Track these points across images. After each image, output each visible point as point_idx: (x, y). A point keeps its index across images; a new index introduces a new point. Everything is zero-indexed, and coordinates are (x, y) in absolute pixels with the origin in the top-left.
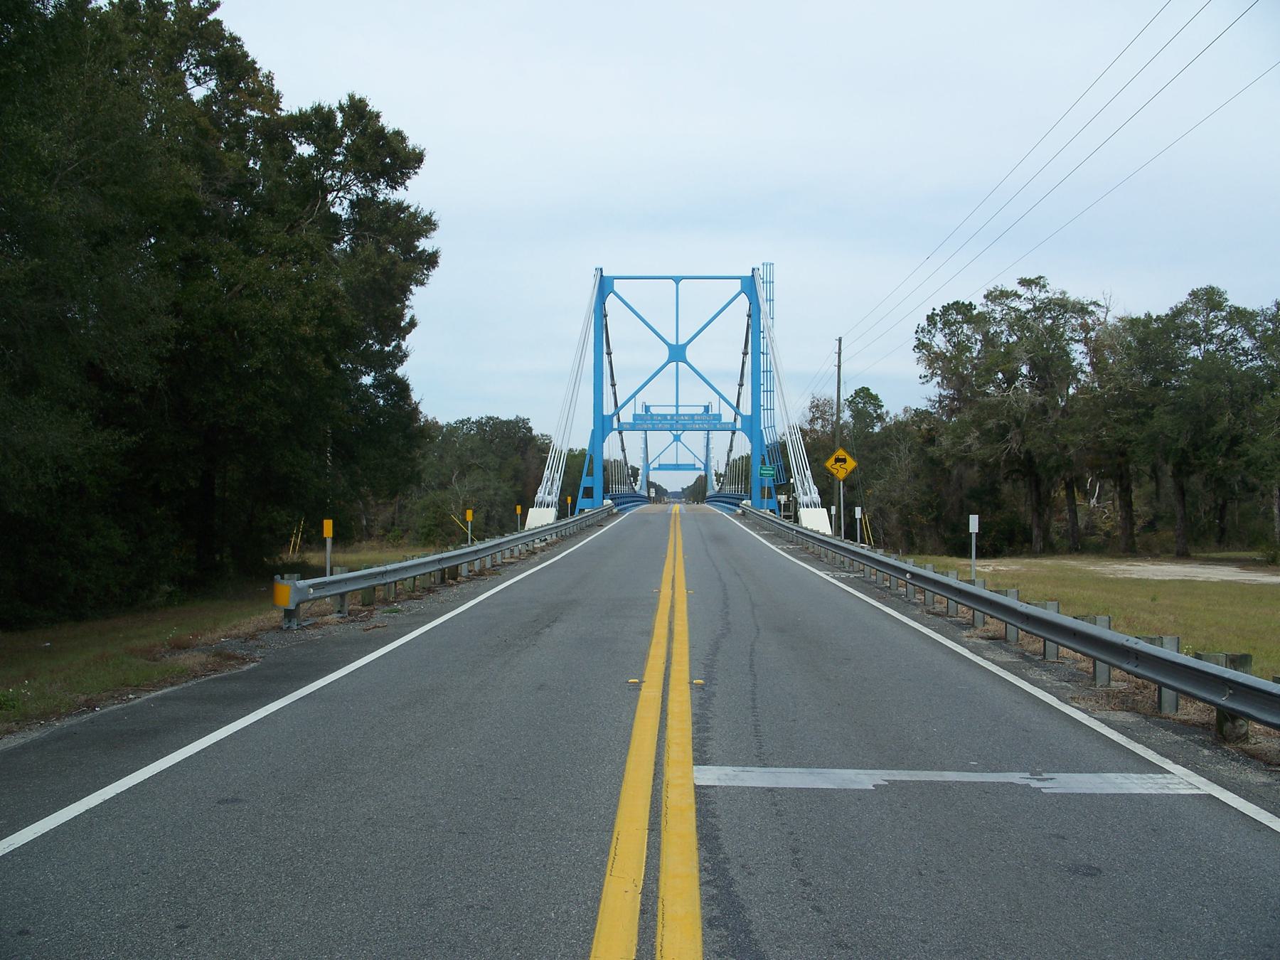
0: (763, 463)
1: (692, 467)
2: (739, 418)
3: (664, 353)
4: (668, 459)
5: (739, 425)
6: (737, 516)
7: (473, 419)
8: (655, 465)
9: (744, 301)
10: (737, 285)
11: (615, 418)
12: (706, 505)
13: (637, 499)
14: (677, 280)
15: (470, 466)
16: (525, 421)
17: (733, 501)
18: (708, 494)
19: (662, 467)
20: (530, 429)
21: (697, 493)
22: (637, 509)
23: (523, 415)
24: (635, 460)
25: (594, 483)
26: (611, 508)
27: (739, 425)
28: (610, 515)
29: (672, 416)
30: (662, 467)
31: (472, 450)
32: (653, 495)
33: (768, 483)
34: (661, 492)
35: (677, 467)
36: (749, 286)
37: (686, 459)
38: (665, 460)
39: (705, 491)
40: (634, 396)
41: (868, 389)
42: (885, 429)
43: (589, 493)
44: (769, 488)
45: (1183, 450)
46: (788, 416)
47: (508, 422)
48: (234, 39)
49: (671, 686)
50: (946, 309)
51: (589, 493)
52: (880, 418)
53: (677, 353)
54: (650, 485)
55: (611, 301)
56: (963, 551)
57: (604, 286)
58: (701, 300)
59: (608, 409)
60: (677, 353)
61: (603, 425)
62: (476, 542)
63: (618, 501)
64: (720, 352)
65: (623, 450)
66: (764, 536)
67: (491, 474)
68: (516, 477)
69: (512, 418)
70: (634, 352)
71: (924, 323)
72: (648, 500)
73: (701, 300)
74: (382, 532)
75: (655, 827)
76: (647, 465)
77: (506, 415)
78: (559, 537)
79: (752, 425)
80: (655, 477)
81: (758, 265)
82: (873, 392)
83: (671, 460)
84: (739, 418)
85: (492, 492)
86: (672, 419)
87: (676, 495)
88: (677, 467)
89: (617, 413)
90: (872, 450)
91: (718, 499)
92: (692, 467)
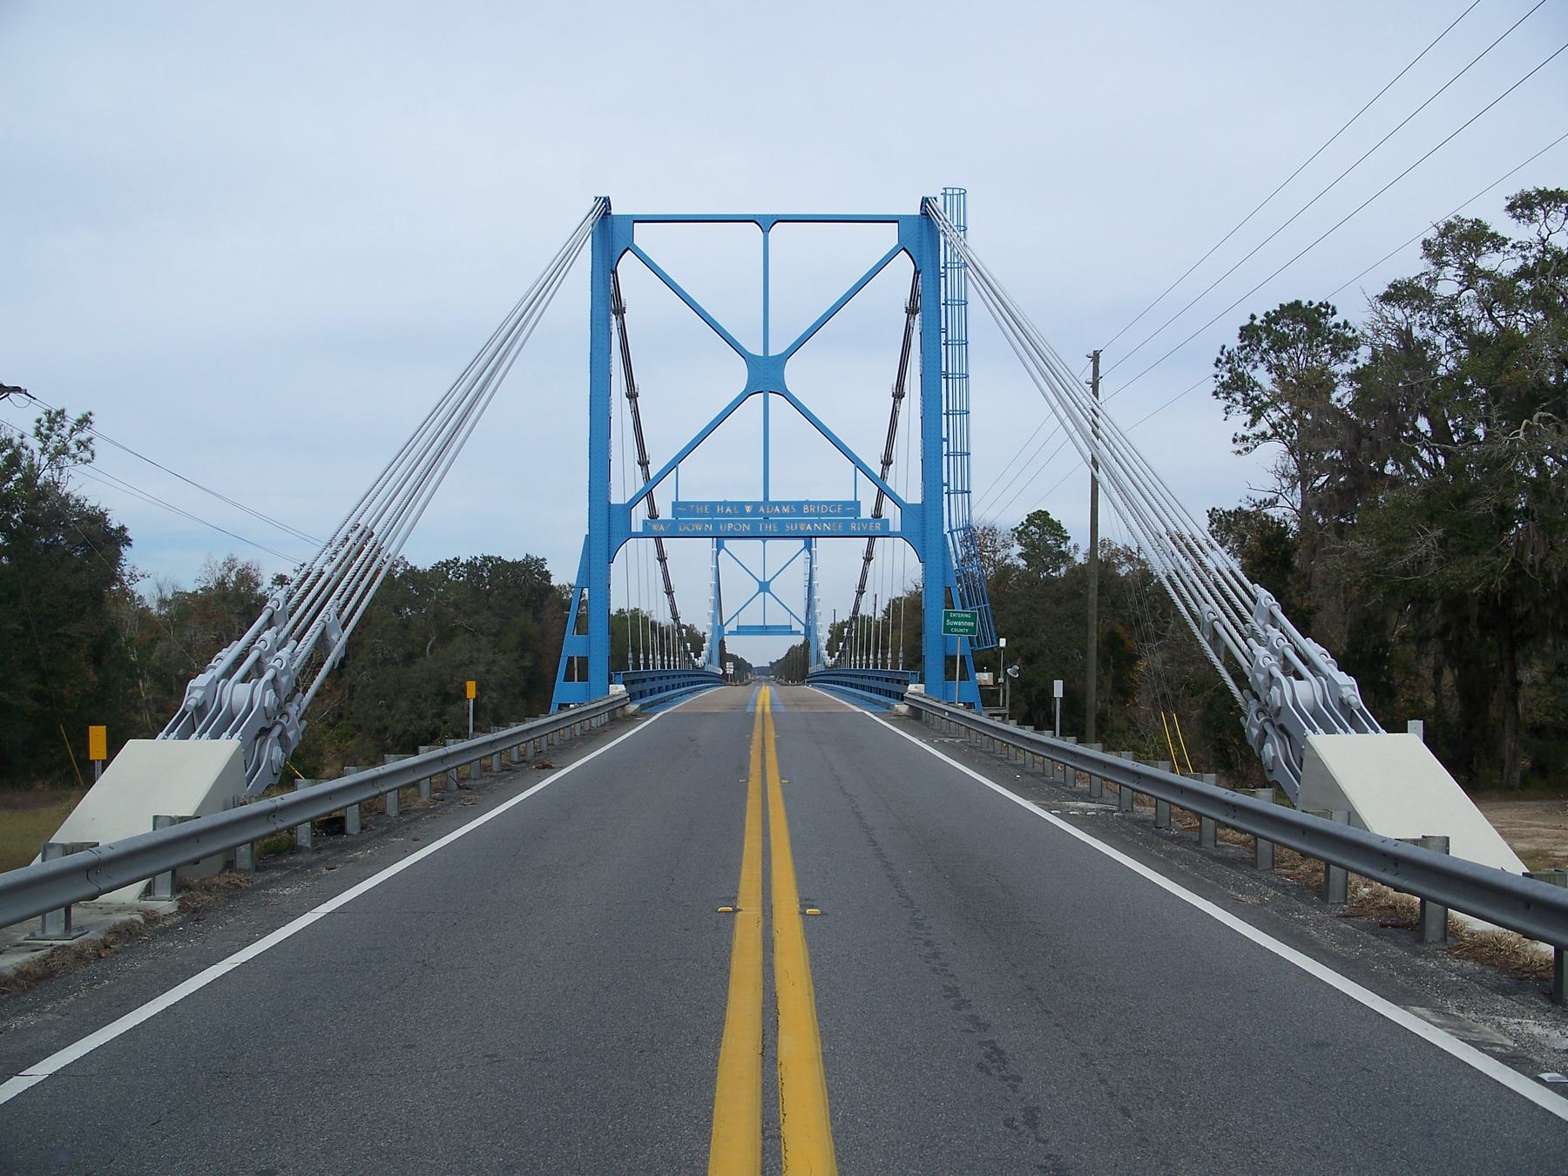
0: (949, 603)
4: (752, 617)
6: (898, 719)
7: (463, 561)
8: (732, 627)
9: (903, 266)
10: (889, 235)
12: (809, 687)
13: (701, 678)
14: (766, 223)
15: (452, 630)
16: (540, 563)
17: (886, 688)
18: (812, 669)
19: (741, 630)
20: (547, 576)
21: (794, 668)
22: (690, 699)
24: (696, 616)
25: (655, 659)
26: (620, 704)
28: (617, 718)
29: (755, 505)
30: (741, 630)
31: (456, 605)
32: (730, 671)
33: (960, 648)
34: (741, 665)
35: (765, 630)
36: (923, 233)
37: (777, 617)
38: (747, 619)
39: (806, 664)
40: (673, 465)
42: (1072, 571)
43: (580, 670)
44: (962, 658)
47: (515, 564)
50: (1271, 319)
51: (580, 670)
52: (1064, 557)
53: (764, 587)
54: (724, 657)
55: (628, 266)
56: (1044, 724)
57: (610, 234)
59: (624, 484)
60: (764, 587)
61: (608, 528)
62: (302, 781)
63: (636, 688)
64: (854, 383)
65: (669, 592)
66: (1081, 821)
67: (484, 641)
68: (524, 644)
70: (682, 384)
71: (1234, 343)
72: (724, 679)
75: (768, 946)
76: (719, 628)
77: (512, 554)
78: (215, 871)
80: (734, 646)
81: (933, 191)
82: (1054, 516)
85: (482, 668)
86: (755, 513)
87: (762, 670)
88: (765, 630)
90: (1058, 602)
91: (829, 678)
92: (839, 520)
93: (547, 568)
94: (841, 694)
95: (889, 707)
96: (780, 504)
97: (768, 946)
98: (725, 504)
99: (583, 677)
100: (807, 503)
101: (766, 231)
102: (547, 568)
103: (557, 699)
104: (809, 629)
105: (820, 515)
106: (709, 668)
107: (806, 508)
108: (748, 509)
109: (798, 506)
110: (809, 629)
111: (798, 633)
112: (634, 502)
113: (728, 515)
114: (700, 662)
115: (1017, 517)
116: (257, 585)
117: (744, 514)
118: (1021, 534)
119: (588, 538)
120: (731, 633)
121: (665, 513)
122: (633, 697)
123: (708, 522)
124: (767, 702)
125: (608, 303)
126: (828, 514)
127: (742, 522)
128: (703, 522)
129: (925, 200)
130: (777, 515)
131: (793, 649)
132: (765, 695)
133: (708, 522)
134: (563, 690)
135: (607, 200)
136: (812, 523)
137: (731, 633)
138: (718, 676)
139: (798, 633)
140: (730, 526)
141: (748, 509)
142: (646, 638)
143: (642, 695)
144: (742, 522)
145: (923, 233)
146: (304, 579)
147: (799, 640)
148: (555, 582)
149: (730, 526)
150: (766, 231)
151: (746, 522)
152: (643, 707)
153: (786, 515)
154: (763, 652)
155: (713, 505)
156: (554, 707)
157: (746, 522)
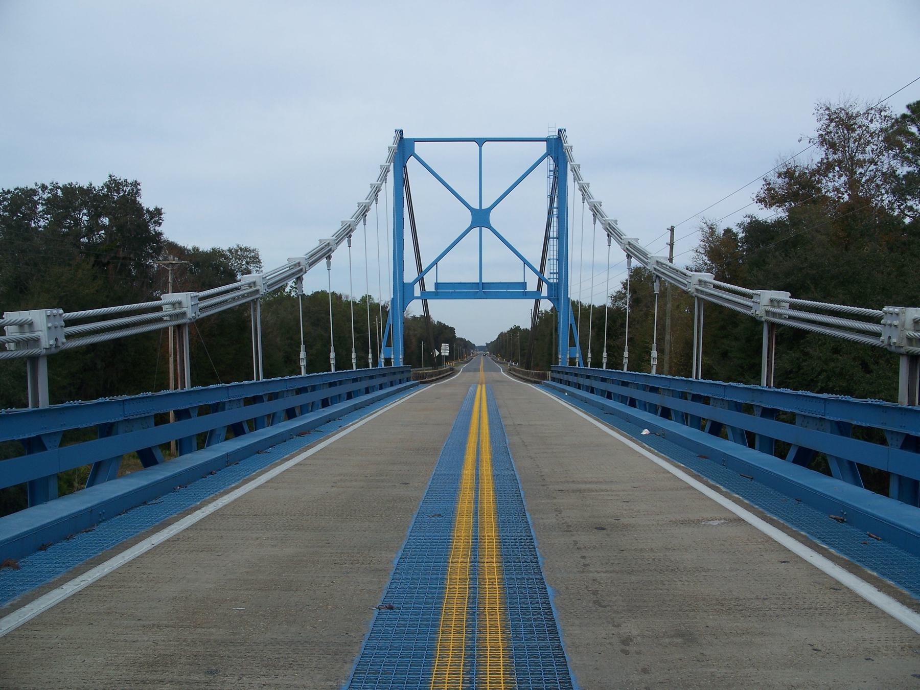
1: (516, 291)
2: (545, 286)
3: (467, 218)
5: (545, 292)
9: (548, 164)
10: (542, 147)
11: (417, 287)
14: (480, 142)
21: (528, 352)
23: (124, 174)
27: (545, 292)
35: (481, 290)
37: (502, 268)
40: (435, 263)
46: (597, 282)
48: (438, 322)
53: (481, 218)
55: (412, 163)
57: (403, 149)
59: (410, 274)
60: (481, 218)
61: (403, 292)
64: (524, 216)
75: (477, 489)
79: (558, 291)
83: (477, 323)
84: (545, 286)
87: (481, 348)
88: (481, 290)
89: (421, 279)
92: (516, 291)
94: (574, 399)
97: (477, 489)
101: (480, 146)
112: (415, 282)
121: (430, 287)
125: (402, 182)
129: (560, 131)
131: (908, 173)
132: (479, 392)
135: (401, 131)
145: (557, 148)
146: (697, 398)
150: (480, 146)
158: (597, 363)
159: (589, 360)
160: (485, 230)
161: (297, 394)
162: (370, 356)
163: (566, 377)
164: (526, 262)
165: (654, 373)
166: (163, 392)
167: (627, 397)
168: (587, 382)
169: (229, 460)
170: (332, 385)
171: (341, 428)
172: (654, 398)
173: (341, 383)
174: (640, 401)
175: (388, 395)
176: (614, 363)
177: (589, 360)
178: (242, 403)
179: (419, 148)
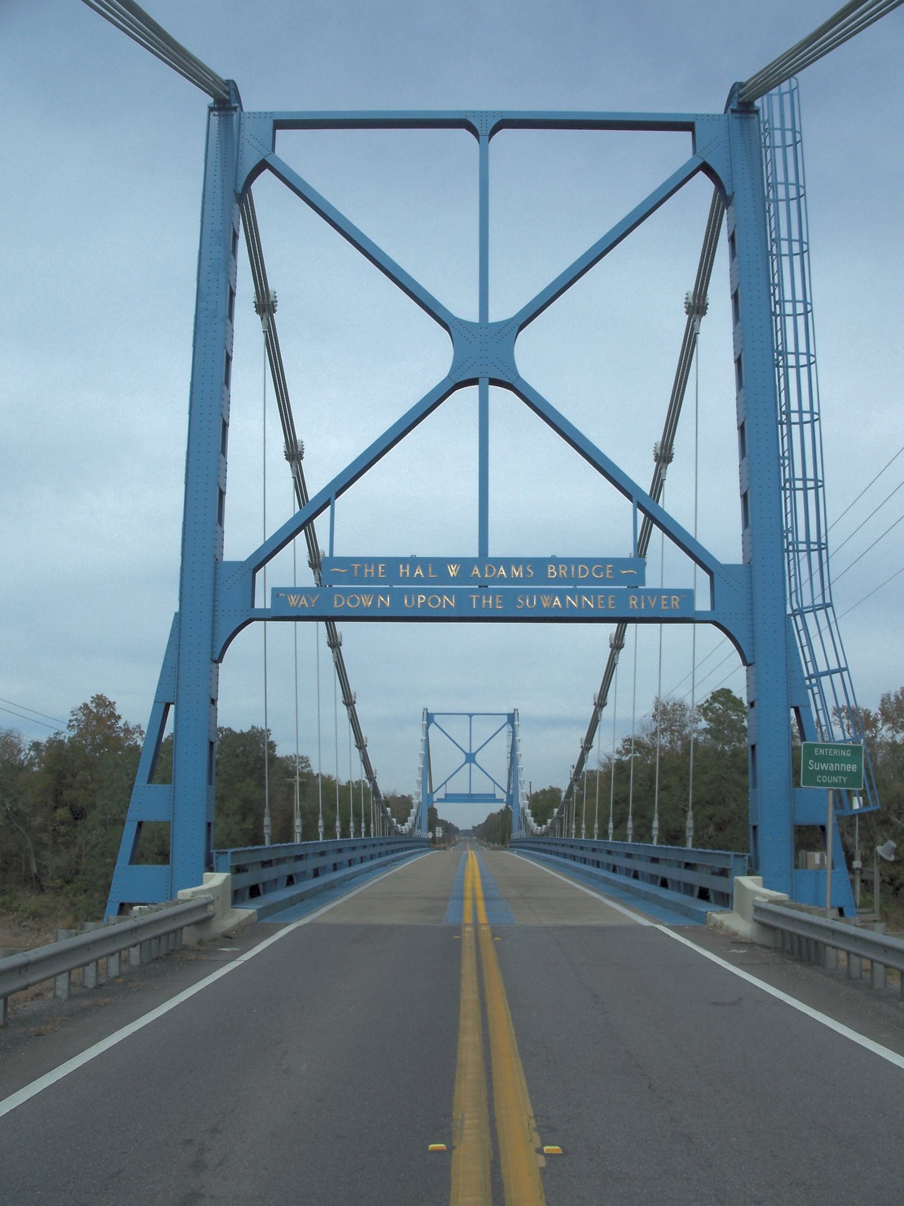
3: (463, 758)
4: (458, 786)
6: (728, 943)
8: (440, 794)
9: (508, 728)
10: (505, 719)
12: (514, 855)
13: (410, 844)
14: (471, 715)
18: (516, 834)
19: (450, 798)
20: (272, 746)
21: (497, 832)
24: (397, 779)
26: (201, 916)
29: (465, 564)
30: (450, 798)
34: (449, 829)
35: (470, 798)
37: (482, 786)
40: (445, 783)
41: (729, 692)
45: (211, 870)
47: (242, 735)
49: (475, 615)
51: (155, 848)
53: (470, 758)
54: (433, 821)
57: (429, 718)
58: (483, 729)
59: (255, 504)
60: (470, 758)
61: (215, 601)
64: (494, 758)
69: (246, 729)
72: (433, 843)
73: (483, 729)
74: (59, 882)
76: (428, 797)
80: (445, 812)
83: (467, 817)
87: (466, 833)
88: (470, 798)
91: (534, 845)
92: (490, 798)
93: (271, 738)
95: (703, 918)
96: (507, 562)
98: (414, 561)
99: (164, 856)
100: (554, 561)
102: (271, 738)
103: (115, 898)
104: (511, 798)
105: (576, 581)
106: (417, 832)
107: (551, 569)
108: (453, 571)
109: (539, 565)
110: (511, 798)
111: (501, 801)
113: (419, 580)
114: (405, 828)
115: (703, 695)
116: (20, 751)
117: (444, 577)
118: (705, 710)
119: (179, 618)
120: (439, 800)
122: (237, 897)
123: (384, 592)
124: (478, 885)
126: (590, 580)
127: (441, 593)
128: (376, 593)
130: (502, 580)
131: (491, 817)
132: (473, 861)
133: (384, 592)
134: (129, 879)
136: (562, 594)
137: (439, 800)
138: (427, 841)
139: (501, 801)
140: (421, 599)
141: (453, 571)
142: (367, 806)
143: (255, 892)
144: (441, 593)
145: (512, 718)
147: (497, 808)
148: (280, 752)
149: (421, 599)
151: (449, 593)
152: (263, 913)
153: (517, 581)
154: (467, 817)
155: (392, 563)
156: (112, 908)
157: (449, 593)
158: (604, 834)
159: (596, 831)
160: (473, 765)
161: (296, 861)
162: (363, 825)
163: (579, 853)
164: (495, 783)
165: (596, 839)
166: (290, 844)
167: (657, 877)
168: (610, 859)
169: (371, 869)
170: (267, 864)
171: (334, 898)
172: (688, 876)
173: (279, 861)
174: (672, 880)
175: (371, 869)
176: (642, 833)
177: (596, 831)
178: (259, 865)
179: (436, 718)
